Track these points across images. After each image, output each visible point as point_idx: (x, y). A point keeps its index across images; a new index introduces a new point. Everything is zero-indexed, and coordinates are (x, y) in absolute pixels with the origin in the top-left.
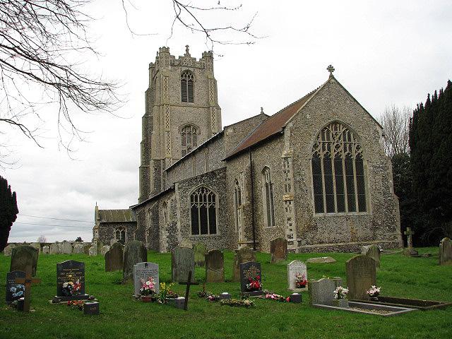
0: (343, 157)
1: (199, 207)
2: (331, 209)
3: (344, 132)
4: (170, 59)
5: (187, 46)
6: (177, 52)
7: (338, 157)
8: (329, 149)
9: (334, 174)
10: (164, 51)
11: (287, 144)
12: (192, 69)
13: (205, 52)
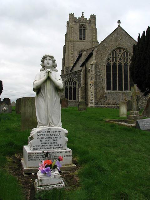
0: (123, 64)
1: (68, 87)
2: (115, 89)
3: (124, 52)
4: (74, 19)
5: (83, 13)
6: (78, 16)
7: (120, 64)
8: (116, 61)
9: (117, 72)
10: (72, 15)
11: (94, 58)
12: (85, 24)
13: (92, 15)
